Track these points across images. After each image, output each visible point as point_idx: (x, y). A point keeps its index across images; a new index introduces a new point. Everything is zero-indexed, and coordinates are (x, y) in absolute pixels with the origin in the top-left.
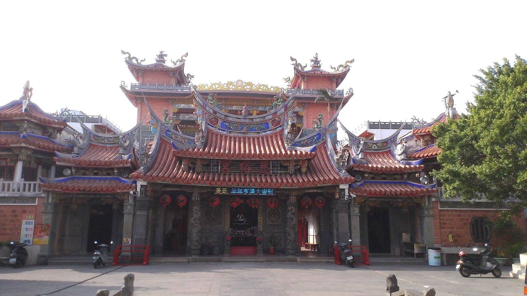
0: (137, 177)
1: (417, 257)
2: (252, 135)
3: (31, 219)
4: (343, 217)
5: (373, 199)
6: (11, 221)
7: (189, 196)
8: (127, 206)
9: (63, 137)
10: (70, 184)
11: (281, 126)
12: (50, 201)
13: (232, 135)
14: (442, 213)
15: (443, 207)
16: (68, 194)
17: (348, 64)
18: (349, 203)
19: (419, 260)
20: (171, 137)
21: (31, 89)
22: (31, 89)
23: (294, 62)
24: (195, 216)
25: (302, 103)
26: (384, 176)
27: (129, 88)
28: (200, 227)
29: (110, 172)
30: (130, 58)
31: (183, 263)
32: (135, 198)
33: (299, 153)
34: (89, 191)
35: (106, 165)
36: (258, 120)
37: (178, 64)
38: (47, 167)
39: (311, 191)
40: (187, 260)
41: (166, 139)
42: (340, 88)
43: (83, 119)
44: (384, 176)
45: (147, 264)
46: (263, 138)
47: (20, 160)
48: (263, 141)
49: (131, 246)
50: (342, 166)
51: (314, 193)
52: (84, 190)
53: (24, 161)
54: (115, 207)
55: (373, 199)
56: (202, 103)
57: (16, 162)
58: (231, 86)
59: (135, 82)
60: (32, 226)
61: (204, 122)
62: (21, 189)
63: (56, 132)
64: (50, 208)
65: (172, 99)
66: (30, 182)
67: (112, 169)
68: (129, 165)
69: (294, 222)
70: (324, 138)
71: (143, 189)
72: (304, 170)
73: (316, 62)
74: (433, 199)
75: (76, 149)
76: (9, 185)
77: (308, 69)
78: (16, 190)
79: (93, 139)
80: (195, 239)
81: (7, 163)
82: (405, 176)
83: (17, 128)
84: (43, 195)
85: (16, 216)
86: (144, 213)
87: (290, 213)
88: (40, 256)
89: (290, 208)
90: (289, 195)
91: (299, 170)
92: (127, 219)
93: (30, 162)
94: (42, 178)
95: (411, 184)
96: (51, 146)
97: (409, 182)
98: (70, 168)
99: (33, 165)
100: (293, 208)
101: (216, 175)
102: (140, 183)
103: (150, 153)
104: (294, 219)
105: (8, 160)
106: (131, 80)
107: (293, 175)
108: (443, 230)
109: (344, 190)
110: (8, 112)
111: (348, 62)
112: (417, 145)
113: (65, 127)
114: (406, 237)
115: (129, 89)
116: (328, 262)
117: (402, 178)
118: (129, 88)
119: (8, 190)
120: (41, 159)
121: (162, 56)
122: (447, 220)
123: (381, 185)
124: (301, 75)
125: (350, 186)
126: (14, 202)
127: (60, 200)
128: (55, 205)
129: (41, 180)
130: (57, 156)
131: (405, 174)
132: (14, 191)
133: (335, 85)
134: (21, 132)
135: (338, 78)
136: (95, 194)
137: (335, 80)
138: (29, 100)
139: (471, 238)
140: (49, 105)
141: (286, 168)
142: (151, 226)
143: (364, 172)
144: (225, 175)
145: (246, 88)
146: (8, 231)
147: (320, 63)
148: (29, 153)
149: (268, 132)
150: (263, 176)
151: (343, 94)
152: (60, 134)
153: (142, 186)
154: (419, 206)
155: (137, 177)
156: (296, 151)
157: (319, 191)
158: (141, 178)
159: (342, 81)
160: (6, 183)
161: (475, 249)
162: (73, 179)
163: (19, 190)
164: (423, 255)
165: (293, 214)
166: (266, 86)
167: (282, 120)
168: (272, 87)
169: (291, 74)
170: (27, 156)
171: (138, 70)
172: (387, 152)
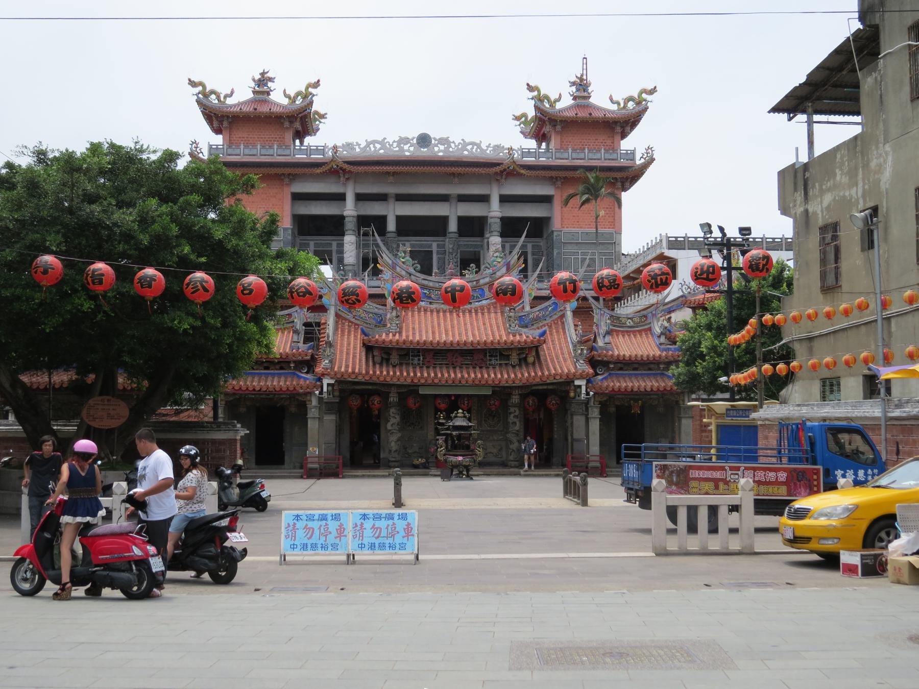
0: (323, 375)
4: (578, 421)
7: (385, 396)
13: (433, 306)
17: (644, 96)
18: (586, 403)
23: (536, 93)
24: (393, 421)
25: (552, 178)
26: (636, 366)
28: (399, 435)
32: (320, 400)
37: (299, 101)
39: (540, 387)
42: (626, 144)
45: (343, 477)
50: (581, 354)
56: (390, 262)
58: (406, 147)
67: (289, 362)
69: (517, 428)
71: (330, 388)
72: (531, 359)
73: (581, 86)
80: (394, 449)
86: (333, 417)
89: (512, 410)
90: (510, 394)
91: (525, 359)
100: (517, 409)
102: (326, 381)
104: (518, 423)
107: (517, 367)
108: (704, 434)
109: (580, 387)
111: (644, 91)
115: (206, 158)
117: (659, 368)
121: (263, 81)
123: (630, 379)
124: (544, 123)
125: (588, 381)
135: (624, 123)
136: (268, 395)
137: (619, 129)
141: (507, 357)
143: (608, 363)
145: (436, 149)
147: (590, 89)
149: (484, 302)
151: (633, 159)
153: (328, 385)
155: (323, 375)
157: (550, 387)
158: (328, 375)
165: (516, 417)
166: (479, 146)
168: (488, 147)
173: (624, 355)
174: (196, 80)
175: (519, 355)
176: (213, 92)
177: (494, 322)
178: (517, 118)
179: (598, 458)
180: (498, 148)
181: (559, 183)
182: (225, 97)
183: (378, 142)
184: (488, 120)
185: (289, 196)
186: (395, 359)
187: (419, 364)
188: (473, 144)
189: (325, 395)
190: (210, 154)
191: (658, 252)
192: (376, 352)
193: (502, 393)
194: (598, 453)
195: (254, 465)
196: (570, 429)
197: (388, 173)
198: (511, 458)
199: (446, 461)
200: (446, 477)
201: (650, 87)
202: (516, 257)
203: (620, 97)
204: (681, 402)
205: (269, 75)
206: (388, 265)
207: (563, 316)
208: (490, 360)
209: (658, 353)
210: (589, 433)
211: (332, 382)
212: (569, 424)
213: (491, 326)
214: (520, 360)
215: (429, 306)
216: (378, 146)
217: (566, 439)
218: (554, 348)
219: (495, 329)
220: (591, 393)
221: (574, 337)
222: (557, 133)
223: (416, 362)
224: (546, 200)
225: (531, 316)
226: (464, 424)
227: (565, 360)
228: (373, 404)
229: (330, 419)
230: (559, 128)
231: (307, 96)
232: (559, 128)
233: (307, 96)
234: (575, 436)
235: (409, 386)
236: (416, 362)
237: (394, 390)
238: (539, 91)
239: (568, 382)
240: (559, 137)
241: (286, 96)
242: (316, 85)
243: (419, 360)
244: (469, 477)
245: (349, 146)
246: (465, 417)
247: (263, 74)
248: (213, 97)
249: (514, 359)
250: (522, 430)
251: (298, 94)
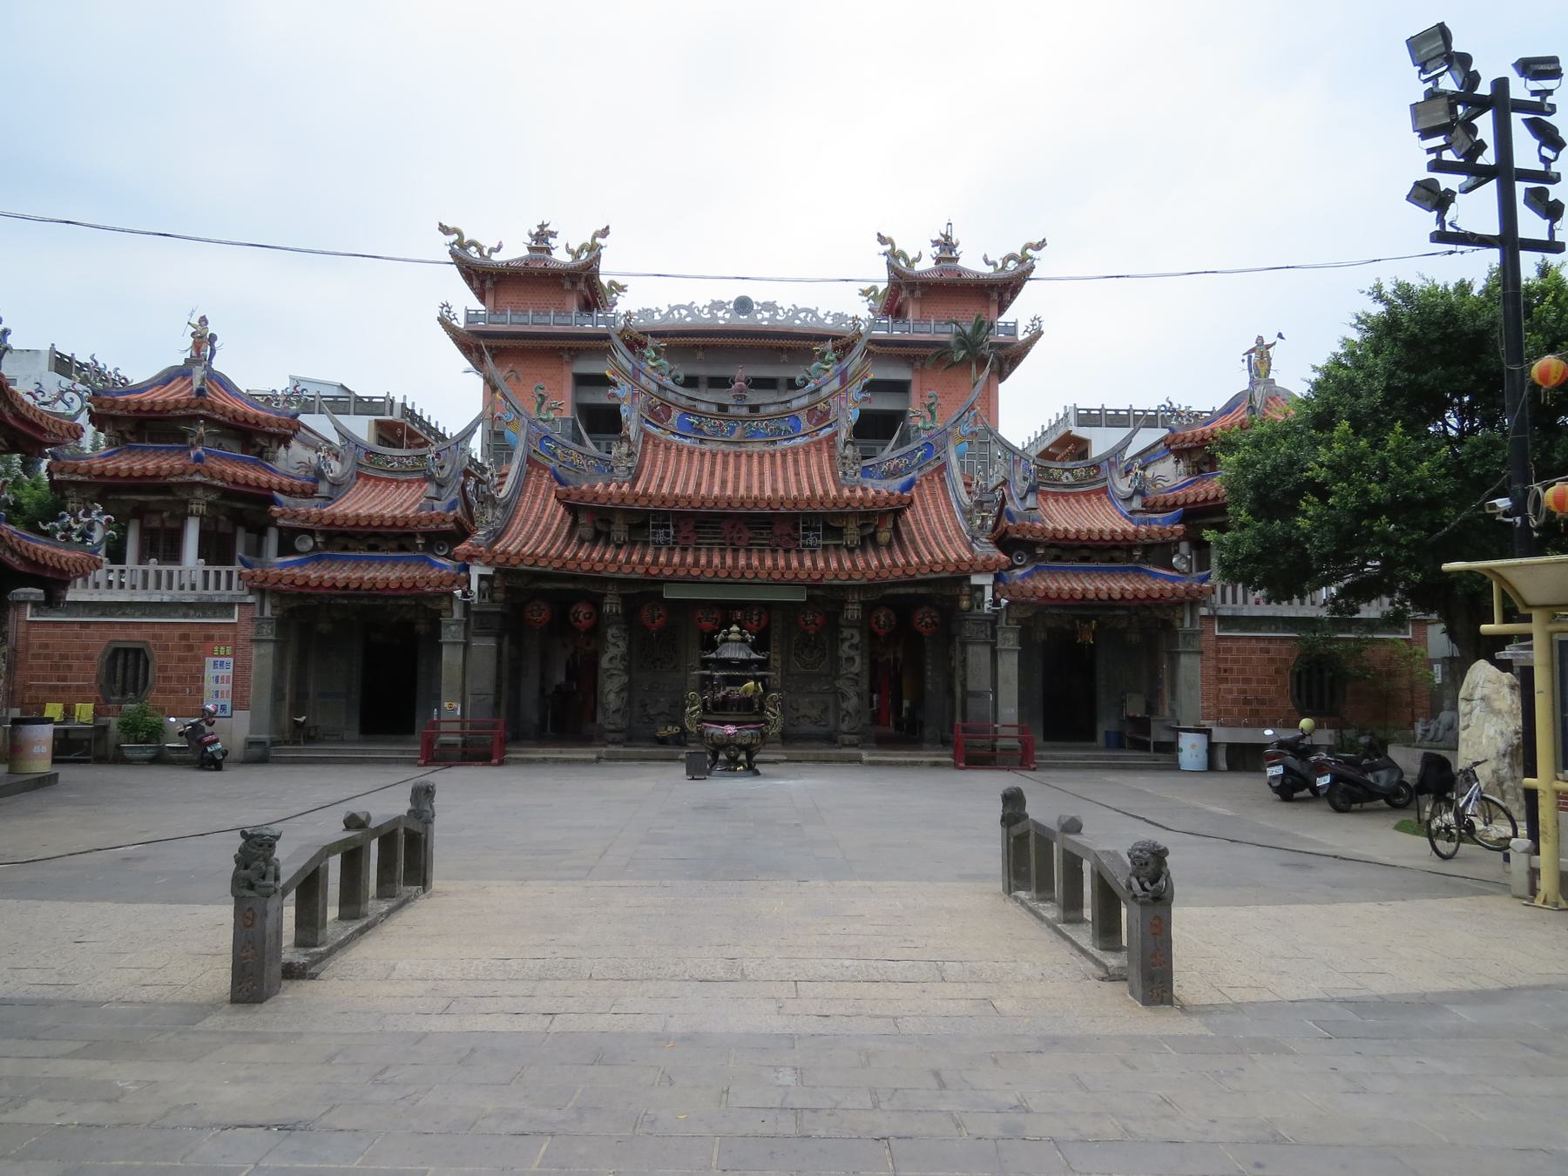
0: (470, 557)
1: (1156, 750)
2: (757, 448)
3: (225, 656)
4: (978, 656)
5: (1055, 611)
6: (180, 659)
7: (596, 602)
8: (448, 625)
9: (293, 458)
10: (313, 573)
11: (830, 425)
12: (268, 612)
13: (706, 447)
14: (1223, 644)
15: (1225, 630)
16: (309, 596)
17: (1029, 252)
18: (993, 621)
19: (1163, 759)
20: (554, 455)
21: (213, 338)
22: (213, 338)
23: (888, 247)
24: (613, 651)
26: (1086, 553)
27: (460, 323)
28: (625, 679)
29: (406, 542)
30: (463, 245)
31: (586, 762)
32: (467, 605)
33: (872, 493)
34: (358, 588)
35: (394, 525)
36: (772, 409)
38: (259, 530)
39: (902, 591)
40: (594, 756)
41: (540, 460)
42: (1007, 317)
43: (344, 402)
44: (1086, 553)
45: (501, 763)
46: (784, 456)
47: (192, 514)
48: (784, 462)
49: (462, 720)
50: (981, 527)
51: (907, 596)
52: (346, 587)
53: (202, 516)
54: (421, 628)
55: (1055, 611)
56: (630, 367)
57: (183, 519)
58: (720, 314)
59: (475, 304)
60: (228, 672)
61: (635, 416)
62: (200, 584)
63: (275, 445)
64: (268, 632)
65: (570, 349)
66: (217, 568)
67: (412, 536)
68: (449, 526)
69: (856, 668)
70: (941, 454)
71: (484, 584)
72: (884, 536)
73: (946, 245)
74: (1204, 611)
75: (323, 488)
76: (170, 574)
77: (926, 265)
78: (187, 586)
79: (364, 461)
80: (613, 707)
81: (163, 522)
82: (1137, 553)
83: (183, 437)
84: (250, 599)
85: (190, 648)
86: (490, 642)
87: (847, 644)
88: (251, 743)
89: (846, 633)
90: (842, 604)
91: (873, 537)
92: (451, 658)
93: (217, 521)
94: (247, 558)
95: (1151, 574)
96: (264, 478)
97: (1146, 567)
98: (311, 533)
99: (224, 526)
100: (855, 632)
101: (664, 550)
102: (476, 571)
103: (502, 495)
105: (165, 515)
106: (465, 301)
109: (981, 588)
110: (158, 396)
112: (1168, 473)
113: (296, 431)
114: (1135, 707)
116: (936, 764)
117: (1130, 558)
118: (460, 323)
119: (170, 587)
120: (242, 510)
121: (542, 237)
122: (1235, 661)
123: (1077, 576)
125: (998, 578)
126: (186, 616)
127: (292, 610)
128: (282, 624)
129: (243, 562)
130: (280, 504)
131: (1136, 547)
132: (182, 587)
133: (994, 309)
134: (193, 446)
135: (1002, 289)
136: (373, 597)
137: (995, 296)
138: (208, 367)
139: (1291, 706)
140: (253, 370)
141: (838, 533)
142: (509, 675)
144: (684, 549)
145: (759, 316)
146: (174, 684)
147: (958, 250)
148: (213, 497)
149: (798, 440)
150: (781, 552)
151: (1015, 334)
152: (287, 447)
153: (482, 578)
154: (1168, 626)
155: (470, 557)
156: (864, 490)
157: (922, 590)
159: (1013, 297)
160: (164, 568)
161: (1269, 732)
162: (319, 559)
163: (193, 587)
164: (1171, 748)
166: (814, 313)
167: (834, 409)
168: (827, 315)
169: (880, 277)
170: (209, 504)
171: (484, 277)
172: (1097, 492)
173: (1066, 530)
174: (450, 225)
175: (862, 527)
176: (472, 243)
177: (814, 470)
178: (864, 293)
179: (1015, 732)
180: (839, 317)
181: (918, 364)
182: (490, 251)
183: (683, 307)
184: (822, 277)
185: (571, 378)
186: (619, 531)
187: (666, 543)
188: (807, 311)
189: (475, 598)
190: (468, 322)
191: (1062, 431)
192: (592, 518)
193: (827, 599)
194: (1015, 721)
195: (356, 734)
196: (959, 672)
197: (696, 347)
198: (844, 727)
199: (701, 733)
200: (697, 771)
201: (1036, 241)
202: (858, 360)
203: (997, 256)
204: (1178, 623)
205: (550, 228)
206: (624, 372)
207: (943, 467)
208: (805, 537)
209: (1131, 528)
210: (1000, 682)
211: (489, 571)
212: (956, 662)
213: (810, 477)
214: (863, 539)
215: (698, 446)
216: (684, 312)
217: (950, 691)
218: (928, 521)
219: (816, 480)
220: (1004, 602)
221: (966, 500)
222: (916, 300)
223: (661, 537)
224: (901, 387)
225: (885, 467)
226: (742, 655)
227: (950, 541)
228: (577, 620)
229: (485, 645)
230: (918, 294)
231: (594, 249)
232: (918, 294)
233: (594, 249)
234: (971, 686)
235: (643, 582)
236: (661, 537)
237: (612, 590)
238: (893, 245)
239: (958, 579)
240: (918, 307)
241: (570, 251)
242: (605, 232)
243: (667, 534)
244: (752, 770)
245: (646, 313)
246: (744, 641)
247: (542, 227)
248: (473, 249)
249: (852, 535)
250: (866, 674)
251: (581, 249)
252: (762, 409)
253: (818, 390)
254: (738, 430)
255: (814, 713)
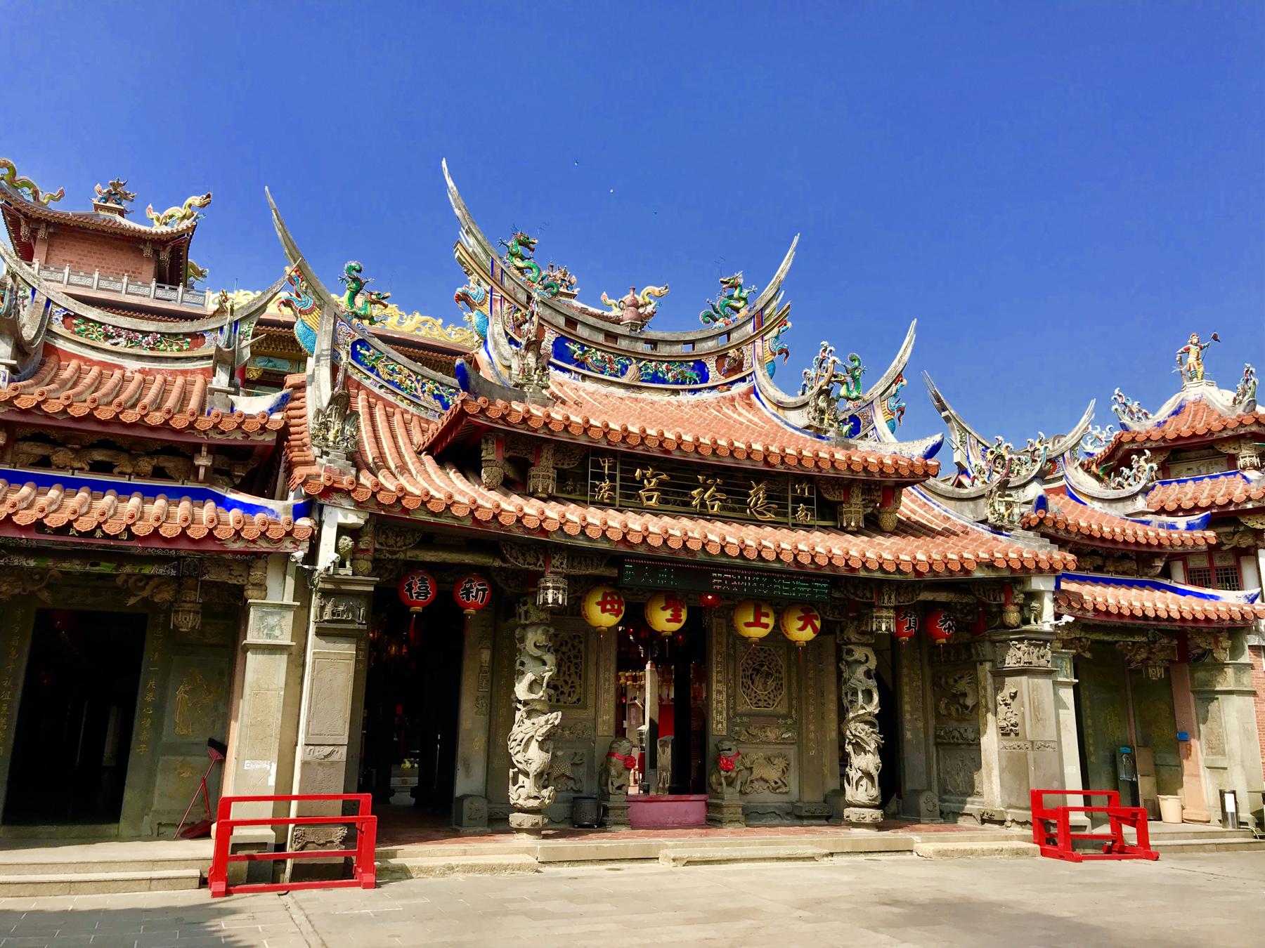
11: (743, 380)
87: (860, 671)
89: (859, 653)
153: (342, 530)
211: (353, 519)
249: (854, 512)
252: (660, 346)
253: (728, 333)
254: (632, 369)
255: (773, 774)
